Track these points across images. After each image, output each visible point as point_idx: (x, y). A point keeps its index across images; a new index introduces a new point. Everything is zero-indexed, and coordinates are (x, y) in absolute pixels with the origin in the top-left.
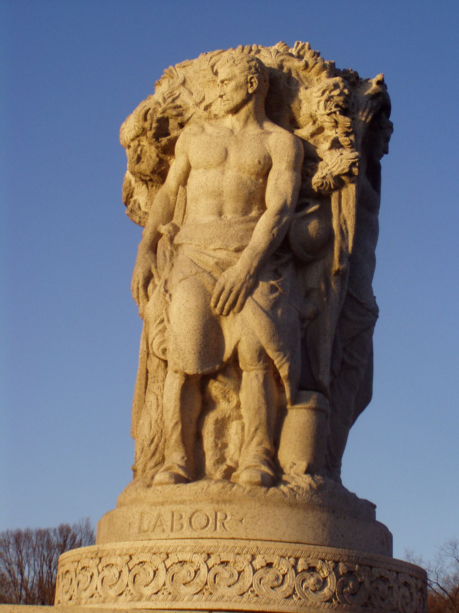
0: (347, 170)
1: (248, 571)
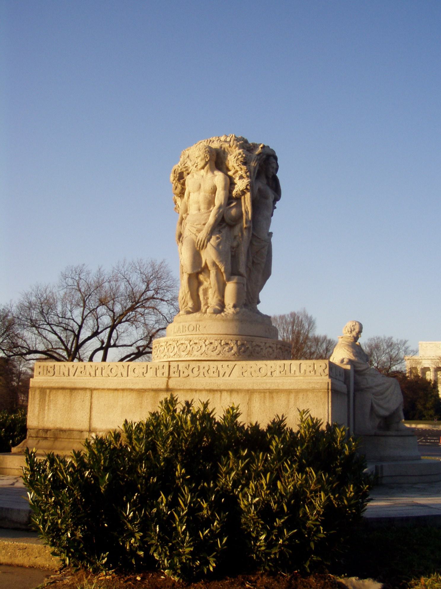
0: (245, 188)
1: (204, 345)
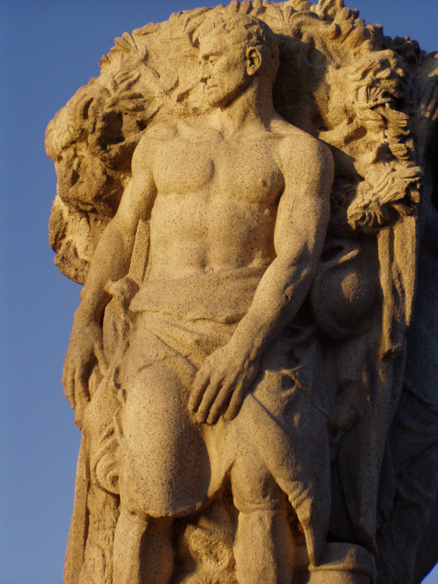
0: (402, 195)
